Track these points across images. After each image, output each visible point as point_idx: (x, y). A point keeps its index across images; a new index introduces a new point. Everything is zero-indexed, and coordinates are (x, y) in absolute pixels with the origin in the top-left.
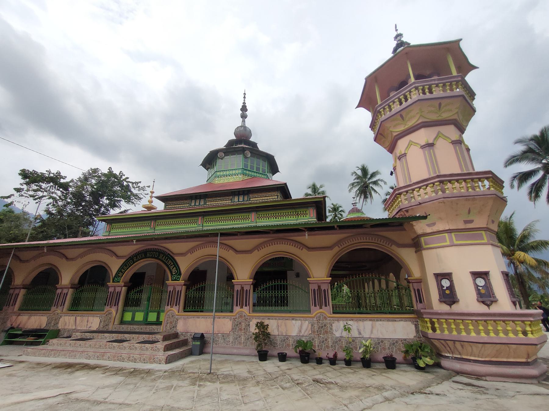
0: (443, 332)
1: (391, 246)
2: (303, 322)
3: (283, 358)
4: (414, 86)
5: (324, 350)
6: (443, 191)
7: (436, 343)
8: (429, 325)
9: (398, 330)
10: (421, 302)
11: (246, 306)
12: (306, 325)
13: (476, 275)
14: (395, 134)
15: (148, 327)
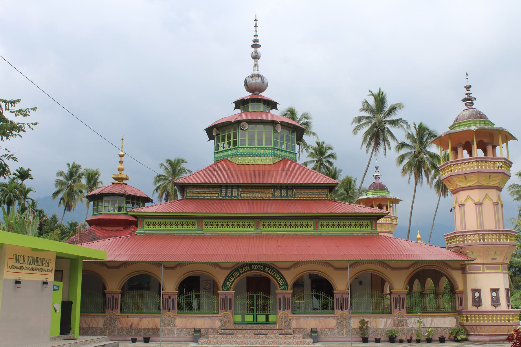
0: (472, 322)
3: (378, 341)
6: (484, 240)
7: (468, 328)
8: (465, 318)
10: (461, 305)
11: (346, 309)
12: (390, 321)
13: (493, 290)
15: (248, 325)
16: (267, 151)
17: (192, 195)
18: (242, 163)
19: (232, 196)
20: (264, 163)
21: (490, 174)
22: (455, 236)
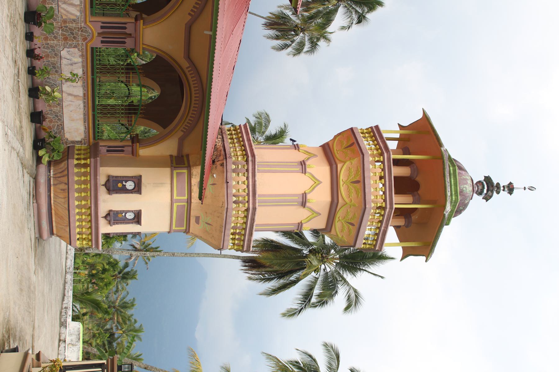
1: (182, 131)
2: (78, 8)
4: (388, 206)
5: (42, 34)
7: (63, 165)
8: (83, 162)
9: (74, 124)
10: (108, 151)
14: (339, 166)
21: (357, 226)
22: (247, 154)
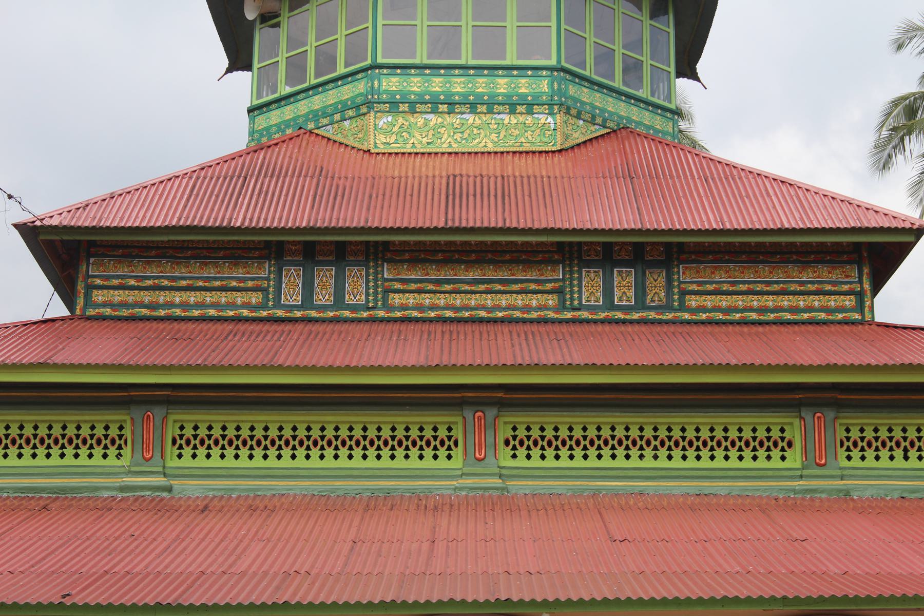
16: (524, 86)
17: (118, 296)
18: (395, 148)
19: (339, 302)
20: (511, 145)
